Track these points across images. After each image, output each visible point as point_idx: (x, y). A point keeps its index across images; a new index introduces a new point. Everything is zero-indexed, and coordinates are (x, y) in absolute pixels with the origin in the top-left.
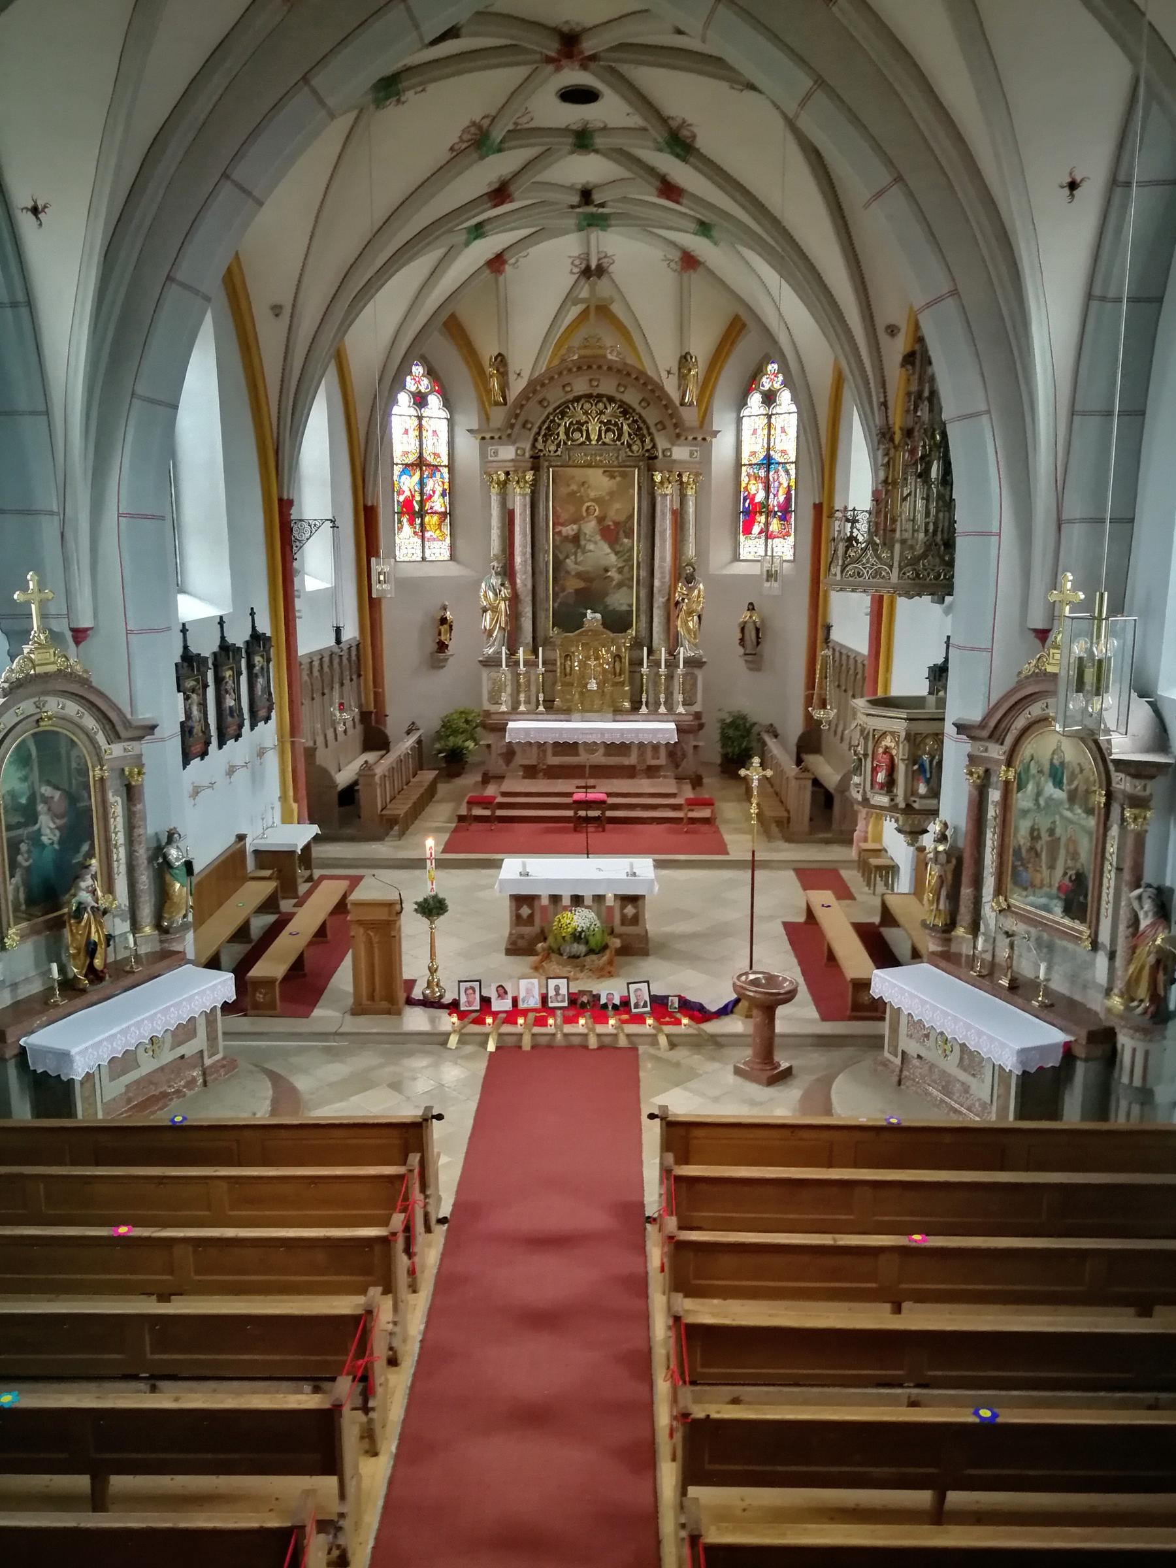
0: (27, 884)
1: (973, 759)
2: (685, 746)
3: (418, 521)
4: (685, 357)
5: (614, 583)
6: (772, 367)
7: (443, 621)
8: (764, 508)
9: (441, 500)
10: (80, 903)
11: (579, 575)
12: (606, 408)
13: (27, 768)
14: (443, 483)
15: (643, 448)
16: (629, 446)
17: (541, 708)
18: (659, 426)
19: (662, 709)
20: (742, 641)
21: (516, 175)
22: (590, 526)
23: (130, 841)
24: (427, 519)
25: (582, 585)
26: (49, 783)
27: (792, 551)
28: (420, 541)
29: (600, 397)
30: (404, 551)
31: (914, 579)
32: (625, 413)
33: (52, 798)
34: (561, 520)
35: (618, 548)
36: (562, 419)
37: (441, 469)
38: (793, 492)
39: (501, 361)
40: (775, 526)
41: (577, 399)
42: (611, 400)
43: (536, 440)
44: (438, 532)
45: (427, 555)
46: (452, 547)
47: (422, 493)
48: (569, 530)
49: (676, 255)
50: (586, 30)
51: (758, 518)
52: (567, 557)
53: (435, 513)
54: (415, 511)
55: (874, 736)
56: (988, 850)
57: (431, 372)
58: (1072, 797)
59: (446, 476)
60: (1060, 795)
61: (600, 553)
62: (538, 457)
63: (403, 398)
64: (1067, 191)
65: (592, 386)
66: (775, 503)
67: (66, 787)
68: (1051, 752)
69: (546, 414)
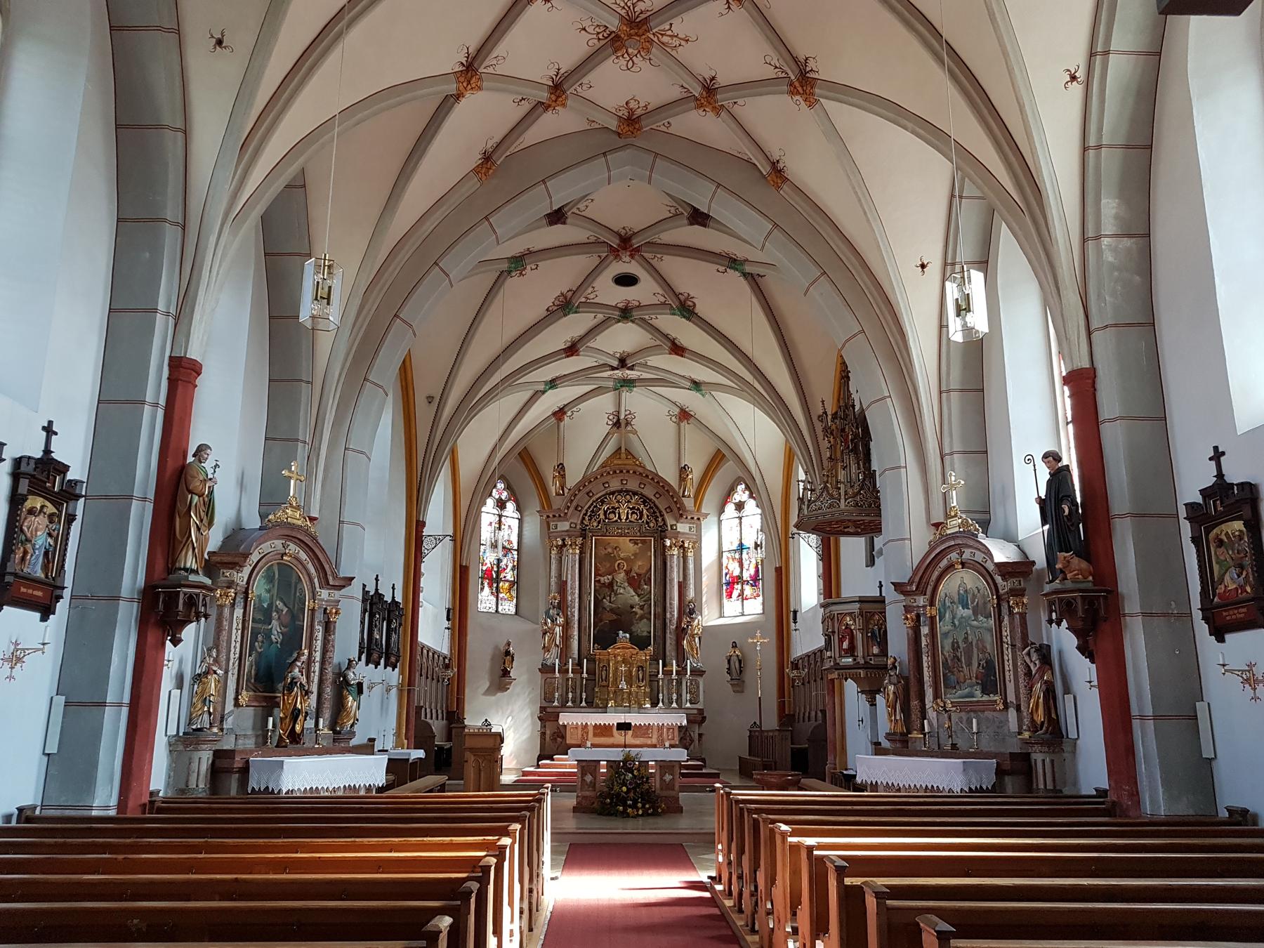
0: (257, 664)
1: (907, 609)
2: (692, 734)
3: (495, 585)
4: (684, 468)
5: (637, 616)
6: (741, 487)
7: (507, 653)
8: (739, 579)
9: (511, 572)
10: (294, 678)
11: (612, 610)
12: (631, 499)
14: (514, 561)
15: (657, 524)
16: (647, 523)
17: (584, 704)
18: (668, 510)
19: (674, 705)
20: (729, 671)
21: (582, 338)
22: (621, 577)
23: (323, 662)
24: (501, 584)
25: (615, 617)
26: (282, 600)
28: (495, 599)
29: (627, 491)
30: (484, 605)
31: (855, 507)
32: (644, 502)
33: (282, 611)
34: (600, 572)
35: (640, 592)
36: (602, 505)
37: (512, 551)
38: (760, 566)
39: (561, 468)
40: (748, 590)
41: (613, 493)
42: (635, 493)
43: (584, 519)
44: (508, 594)
45: (500, 610)
46: (517, 606)
47: (498, 566)
48: (606, 579)
49: (677, 411)
50: (635, 234)
51: (736, 586)
52: (604, 598)
53: (507, 581)
54: (493, 578)
55: (838, 617)
56: (925, 669)
57: (509, 487)
58: (975, 613)
59: (516, 556)
60: (967, 612)
61: (628, 595)
62: (585, 530)
63: (490, 502)
64: (920, 269)
65: (622, 484)
66: (748, 575)
68: (957, 587)
69: (591, 502)
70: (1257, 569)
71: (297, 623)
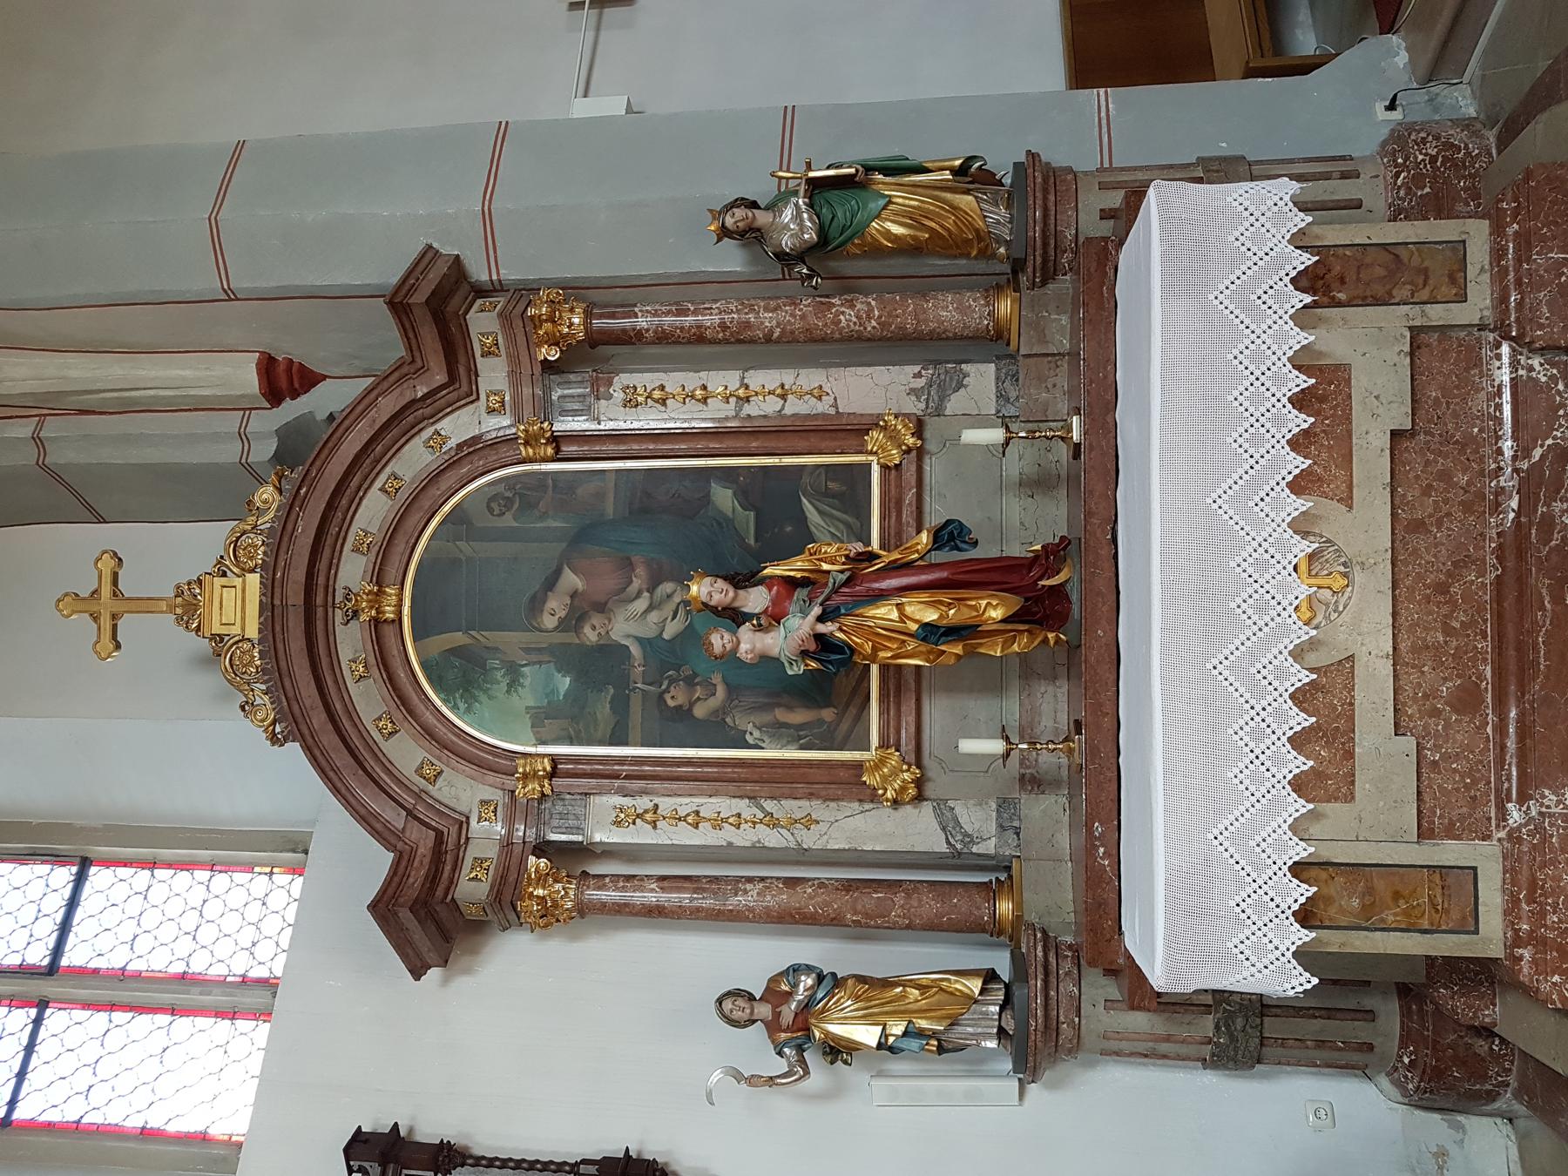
26: (536, 604)
27: (243, 1025)
33: (574, 595)
67: (558, 548)
70: (706, 499)
71: (610, 511)
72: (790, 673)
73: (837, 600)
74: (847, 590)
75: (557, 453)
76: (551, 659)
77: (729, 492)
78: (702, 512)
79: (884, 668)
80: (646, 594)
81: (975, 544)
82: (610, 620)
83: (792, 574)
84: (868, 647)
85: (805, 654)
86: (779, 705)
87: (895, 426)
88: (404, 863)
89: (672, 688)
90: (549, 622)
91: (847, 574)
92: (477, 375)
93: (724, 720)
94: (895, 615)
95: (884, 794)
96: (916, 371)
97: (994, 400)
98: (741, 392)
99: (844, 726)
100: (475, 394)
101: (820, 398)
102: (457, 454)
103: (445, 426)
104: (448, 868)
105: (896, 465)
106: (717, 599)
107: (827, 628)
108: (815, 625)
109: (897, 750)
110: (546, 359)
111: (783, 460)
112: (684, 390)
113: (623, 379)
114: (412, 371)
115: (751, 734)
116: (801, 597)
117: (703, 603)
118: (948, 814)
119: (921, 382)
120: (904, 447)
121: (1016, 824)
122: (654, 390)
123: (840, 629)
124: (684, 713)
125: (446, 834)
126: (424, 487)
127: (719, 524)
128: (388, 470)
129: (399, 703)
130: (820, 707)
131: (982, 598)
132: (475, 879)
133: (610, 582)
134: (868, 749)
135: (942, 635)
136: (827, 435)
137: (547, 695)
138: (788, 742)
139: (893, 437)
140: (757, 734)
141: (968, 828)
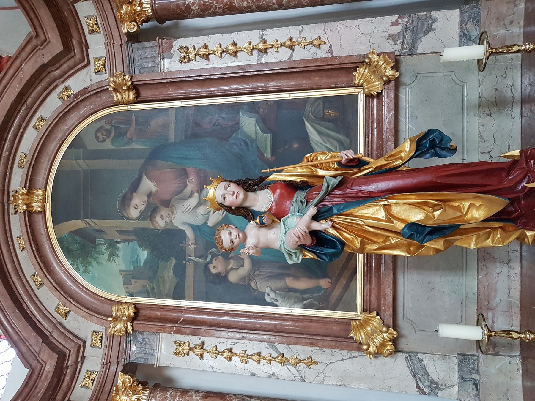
13: (100, 240)
26: (126, 201)
33: (150, 195)
70: (236, 126)
71: (172, 136)
72: (290, 262)
73: (330, 201)
74: (339, 192)
75: (137, 97)
76: (135, 238)
77: (253, 120)
78: (234, 135)
79: (368, 258)
80: (196, 194)
81: (454, 150)
82: (173, 213)
83: (293, 179)
84: (357, 243)
85: (302, 247)
86: (289, 275)
87: (378, 62)
88: (34, 377)
89: (214, 261)
90: (134, 213)
91: (339, 178)
92: (87, 47)
93: (249, 284)
94: (382, 215)
95: (368, 349)
96: (394, 20)
97: (458, 39)
98: (261, 46)
99: (337, 292)
100: (86, 60)
101: (319, 46)
102: (74, 101)
103: (70, 82)
104: (68, 378)
105: (378, 93)
106: (230, 201)
107: (317, 226)
108: (311, 223)
109: (378, 314)
110: (128, 32)
111: (292, 95)
112: (220, 47)
113: (179, 43)
114: (39, 43)
115: (268, 295)
116: (299, 199)
117: (219, 203)
118: (418, 365)
119: (398, 29)
120: (385, 78)
121: (475, 376)
122: (200, 48)
123: (333, 227)
124: (222, 278)
125: (68, 354)
126: (56, 124)
127: (246, 143)
128: (38, 114)
129: (42, 265)
130: (318, 277)
131: (464, 199)
132: (85, 386)
133: (171, 186)
134: (354, 310)
135: (427, 234)
136: (324, 74)
137: (133, 263)
138: (295, 302)
139: (376, 71)
140: (273, 295)
141: (434, 376)
